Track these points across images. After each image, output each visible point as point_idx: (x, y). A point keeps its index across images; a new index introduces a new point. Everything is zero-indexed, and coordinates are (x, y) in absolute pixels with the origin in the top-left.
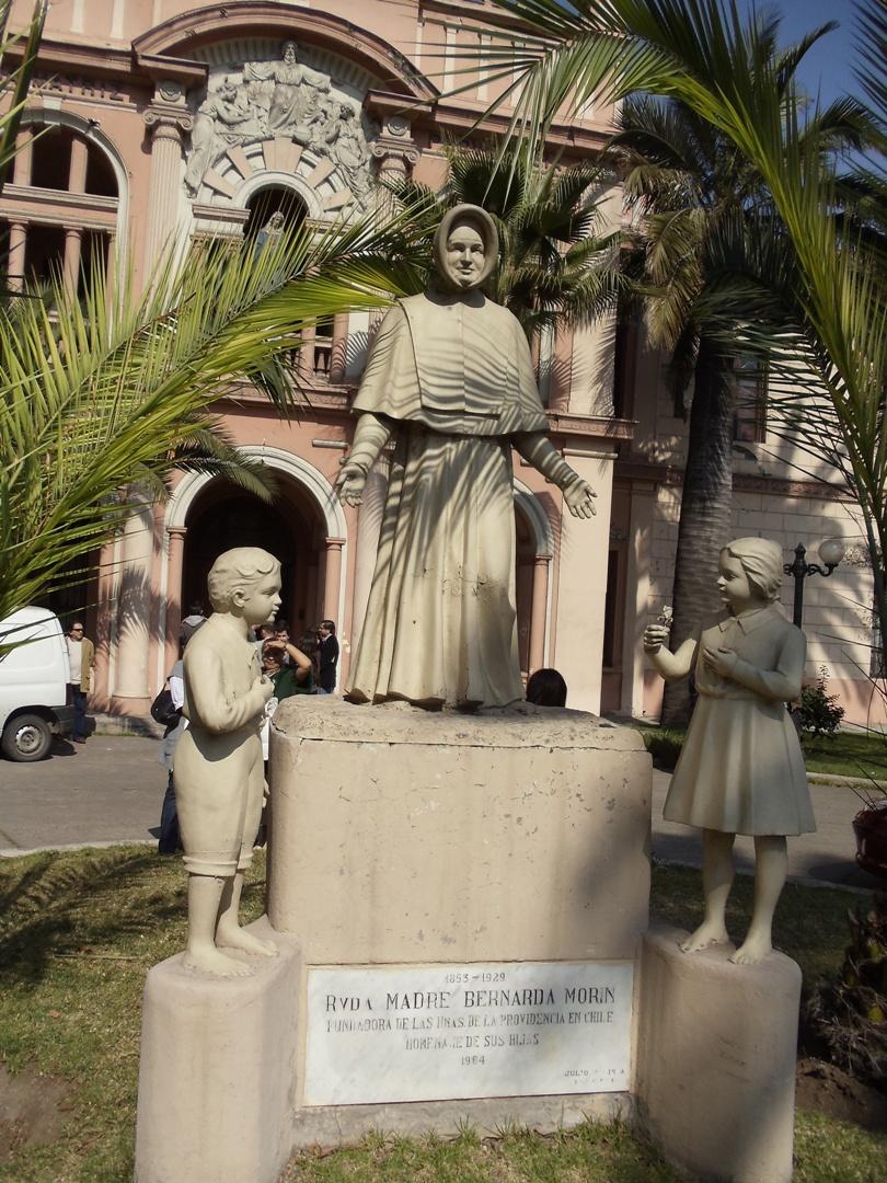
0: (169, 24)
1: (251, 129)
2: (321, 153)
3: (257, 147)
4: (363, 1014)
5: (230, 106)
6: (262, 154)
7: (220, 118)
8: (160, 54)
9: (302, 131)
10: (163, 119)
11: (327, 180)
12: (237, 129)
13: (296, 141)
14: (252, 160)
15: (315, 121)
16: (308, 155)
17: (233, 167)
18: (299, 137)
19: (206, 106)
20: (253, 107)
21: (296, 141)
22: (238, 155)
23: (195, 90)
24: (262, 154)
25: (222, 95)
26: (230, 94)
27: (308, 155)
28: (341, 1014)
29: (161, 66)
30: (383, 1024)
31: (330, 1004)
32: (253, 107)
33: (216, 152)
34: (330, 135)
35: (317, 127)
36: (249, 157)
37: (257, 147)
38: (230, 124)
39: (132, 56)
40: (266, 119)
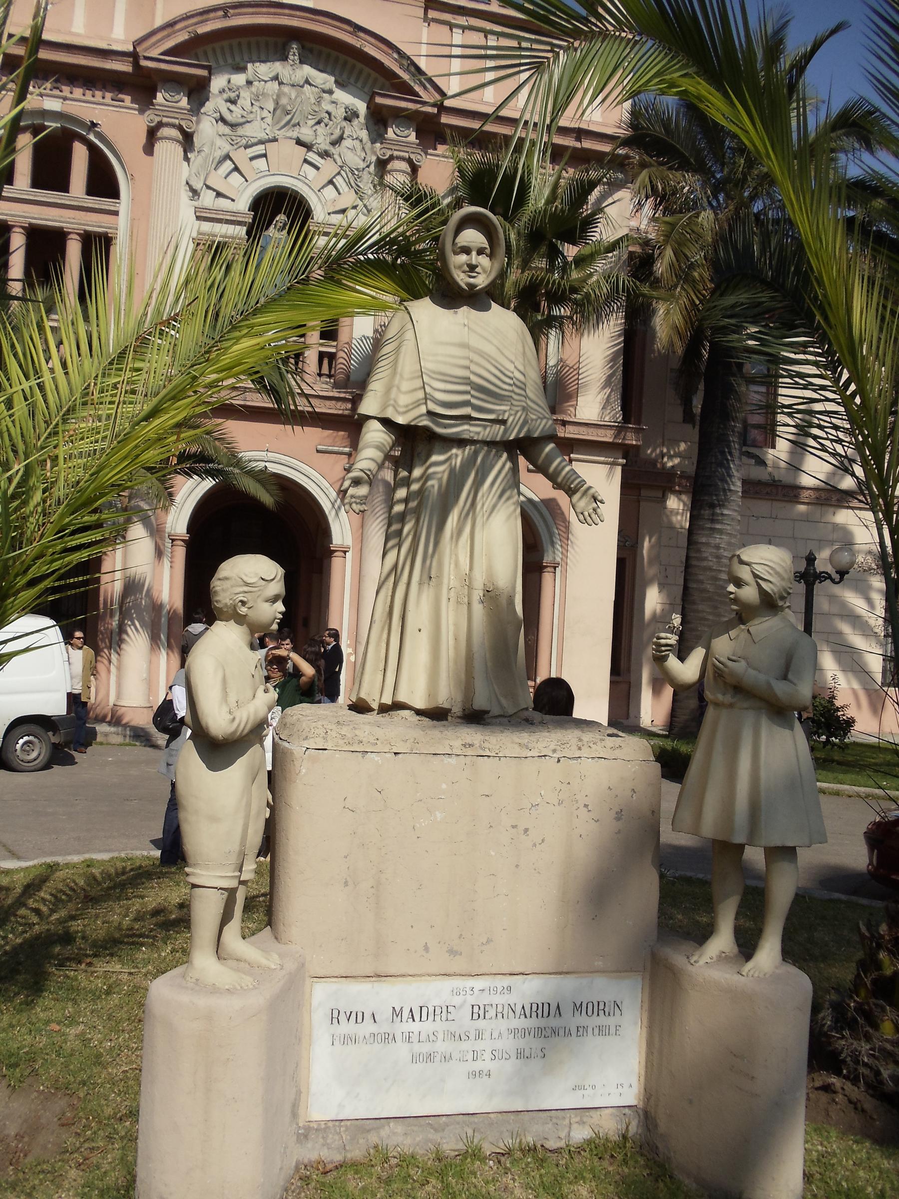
0: (171, 25)
1: (255, 131)
2: (325, 154)
3: (260, 149)
4: (368, 1027)
5: (232, 107)
6: (265, 155)
7: (222, 119)
8: (162, 54)
9: (306, 133)
10: (165, 120)
11: (331, 182)
12: (240, 131)
13: (299, 142)
14: (254, 162)
15: (319, 123)
16: (313, 157)
17: (236, 169)
18: (303, 138)
19: (209, 106)
20: (256, 108)
21: (299, 142)
22: (241, 157)
23: (197, 91)
24: (265, 155)
25: (225, 96)
26: (233, 95)
27: (313, 157)
28: (346, 1028)
29: (163, 66)
30: (388, 1038)
31: (335, 1017)
32: (256, 108)
33: (218, 154)
34: (334, 137)
35: (321, 129)
36: (252, 159)
37: (260, 149)
38: (233, 126)
39: (134, 56)
40: (269, 120)
